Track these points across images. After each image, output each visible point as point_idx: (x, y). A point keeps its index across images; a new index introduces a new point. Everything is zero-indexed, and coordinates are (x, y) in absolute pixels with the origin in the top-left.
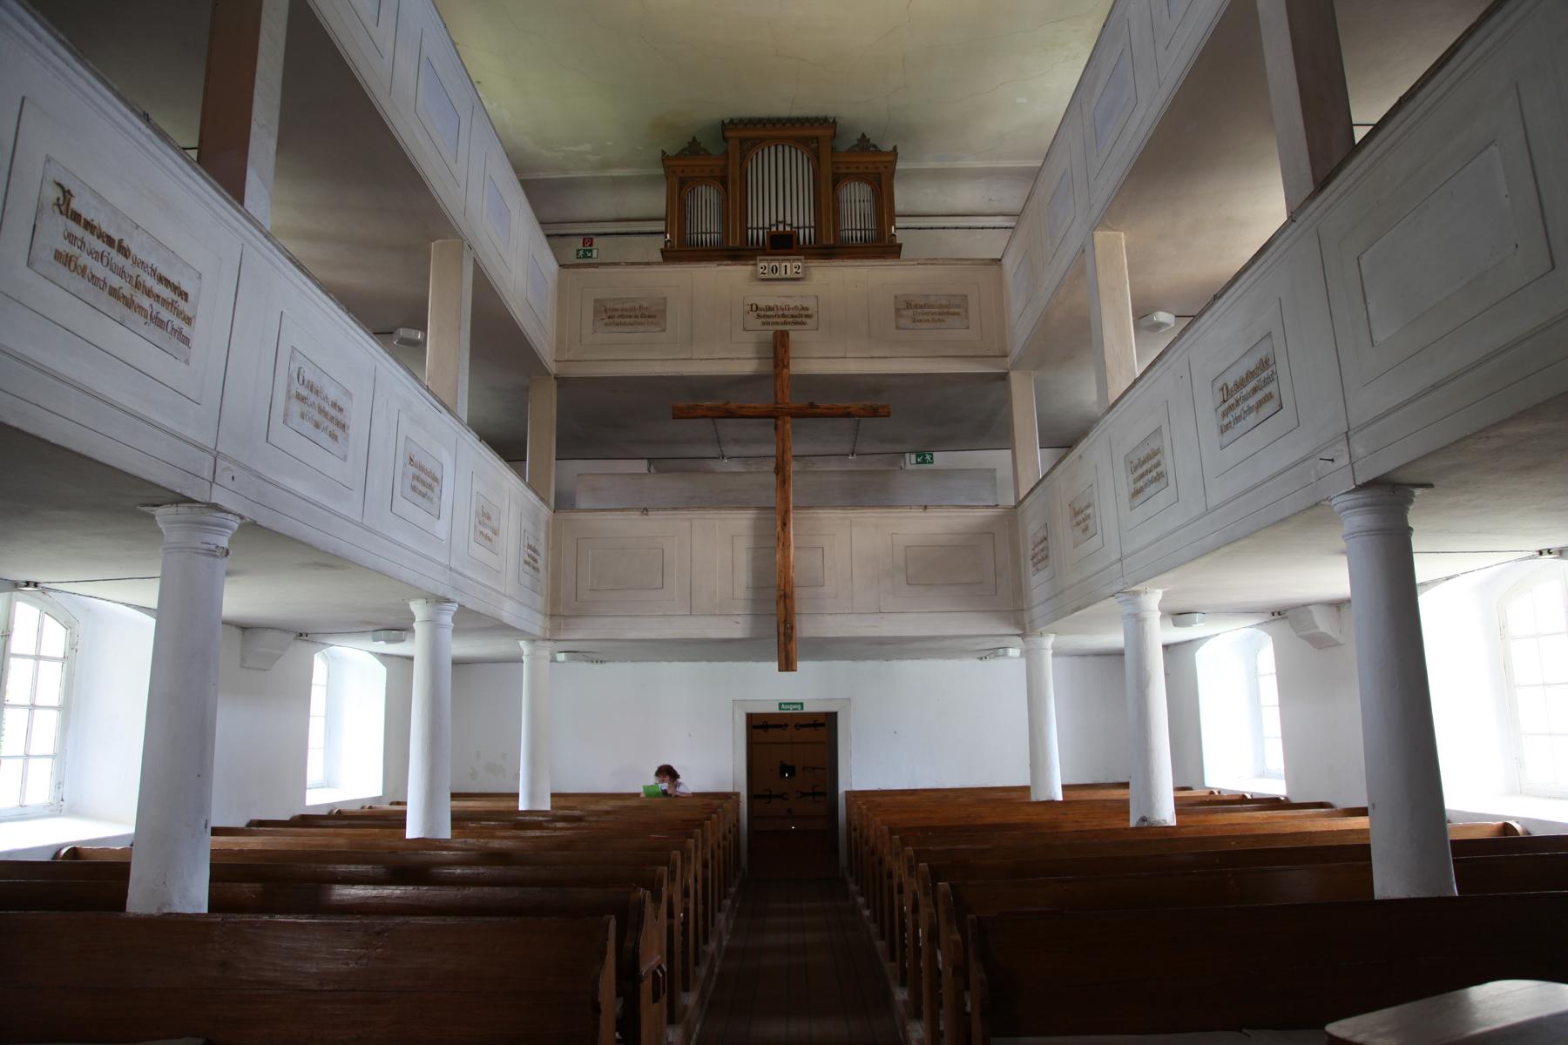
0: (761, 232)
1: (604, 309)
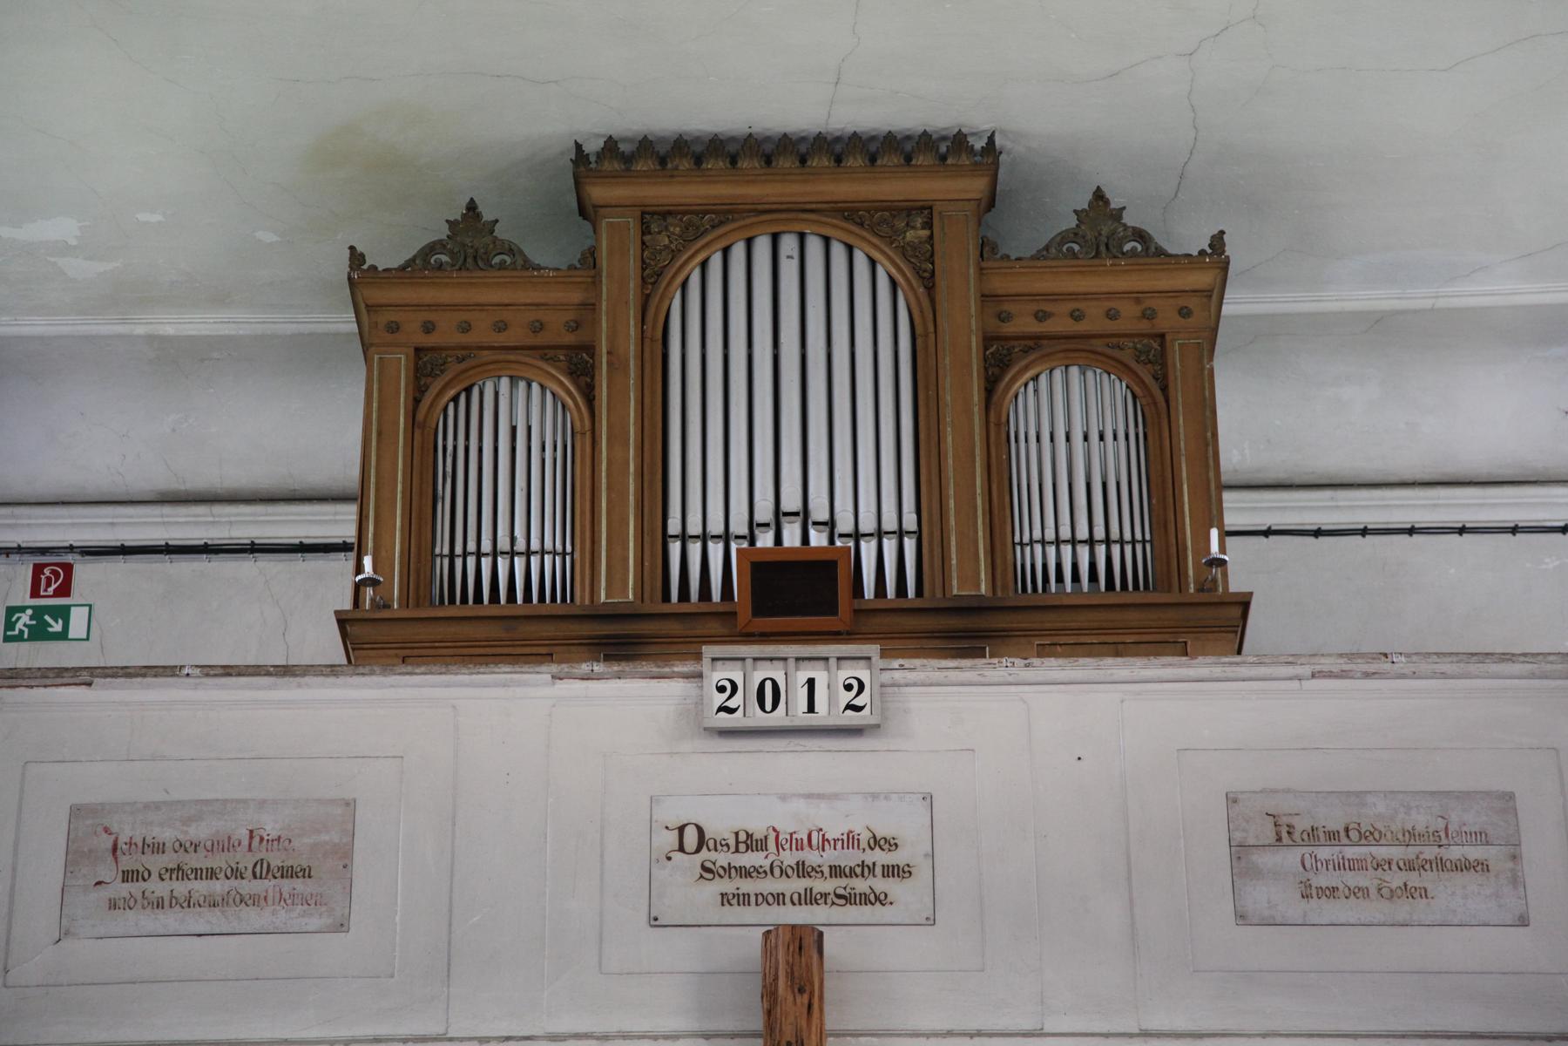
0: (716, 551)
1: (106, 842)
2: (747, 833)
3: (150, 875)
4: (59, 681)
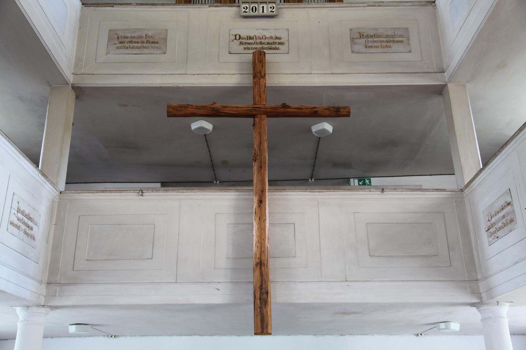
1: (117, 36)
2: (250, 36)
3: (125, 42)
4: (107, 6)
